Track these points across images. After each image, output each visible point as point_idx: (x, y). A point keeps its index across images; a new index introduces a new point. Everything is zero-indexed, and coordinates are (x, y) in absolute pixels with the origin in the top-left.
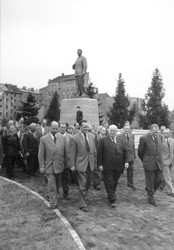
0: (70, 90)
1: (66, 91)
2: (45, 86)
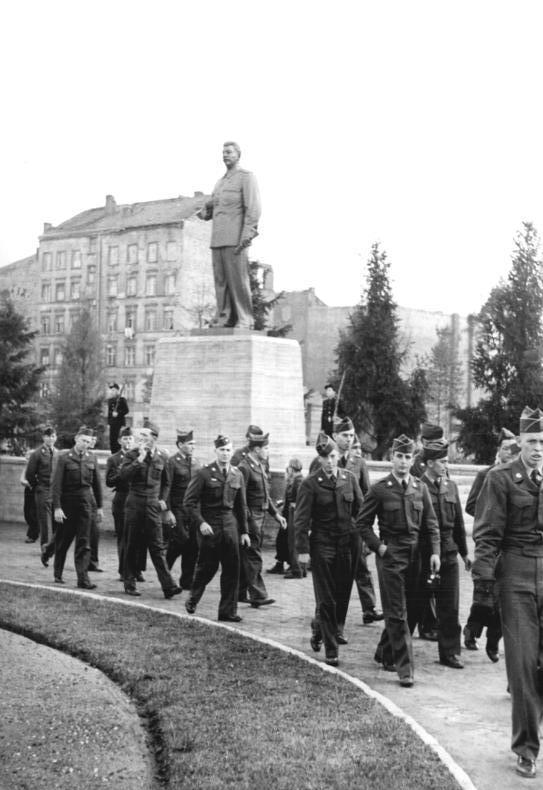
0: (143, 275)
1: (122, 278)
2: (24, 257)
